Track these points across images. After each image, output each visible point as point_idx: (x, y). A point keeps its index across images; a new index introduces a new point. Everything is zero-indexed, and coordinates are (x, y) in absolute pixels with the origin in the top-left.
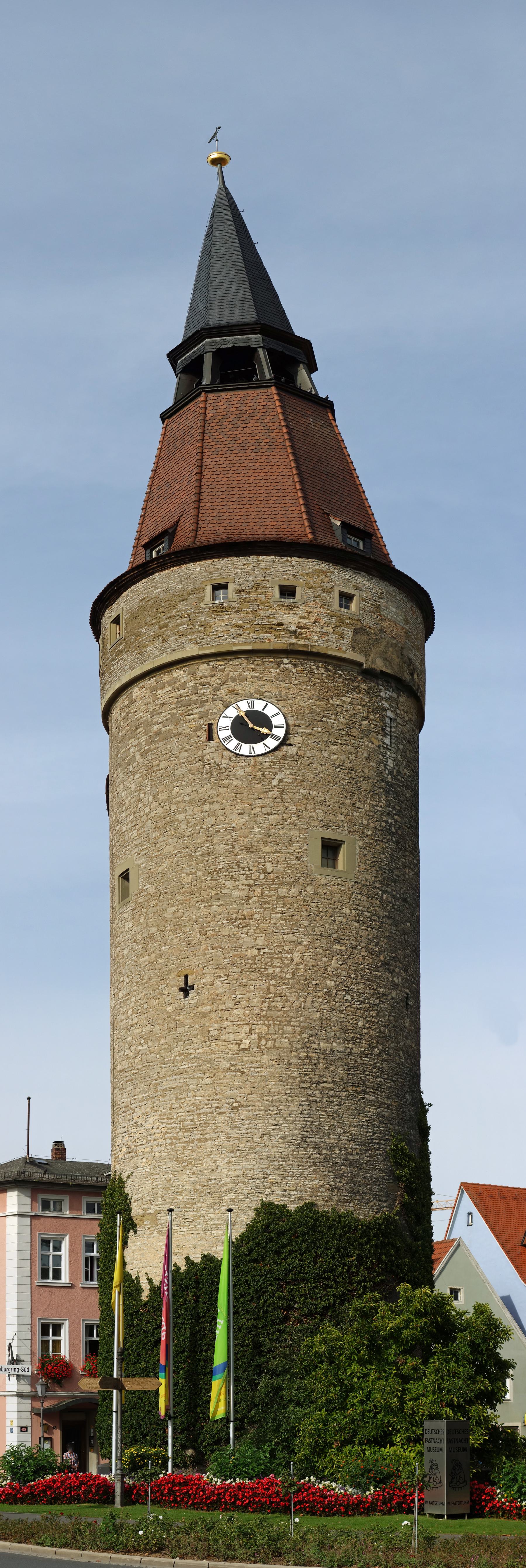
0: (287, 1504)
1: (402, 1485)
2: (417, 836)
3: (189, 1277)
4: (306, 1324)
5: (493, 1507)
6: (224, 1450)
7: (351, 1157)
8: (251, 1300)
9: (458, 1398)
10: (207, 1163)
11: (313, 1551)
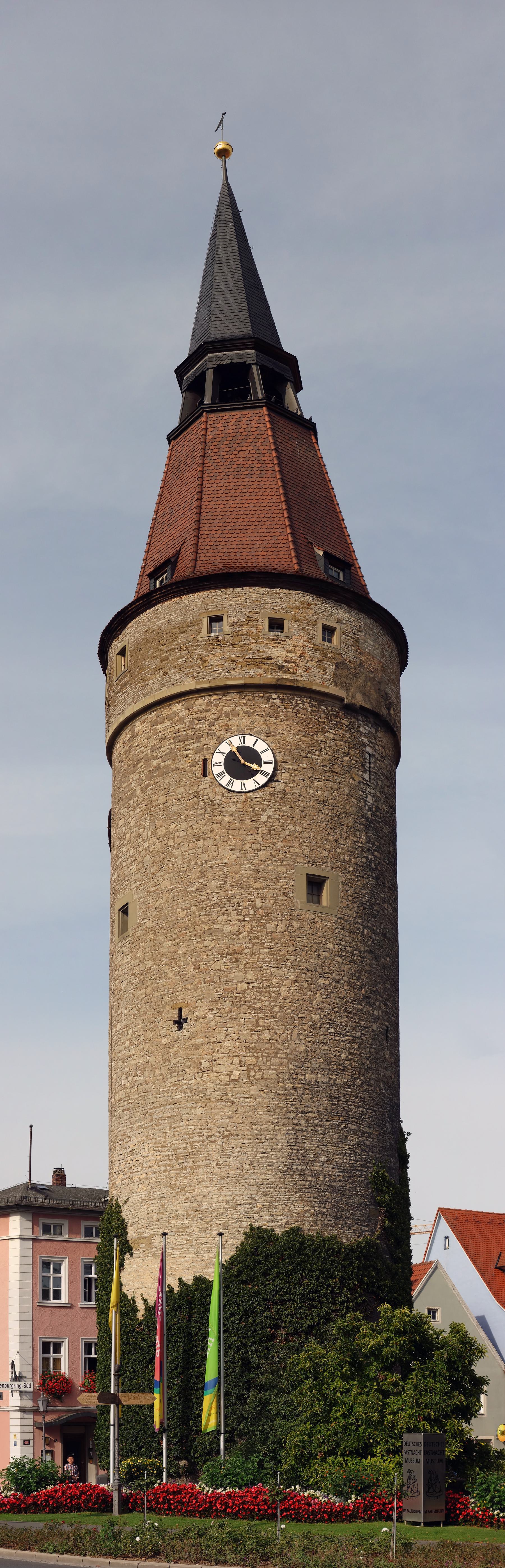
0: (274, 1511)
1: (381, 1494)
2: (395, 871)
3: (182, 1297)
4: (292, 1341)
5: (467, 1515)
6: (215, 1461)
7: (334, 1184)
8: (240, 1320)
9: (435, 1412)
10: (199, 1189)
11: (298, 1556)
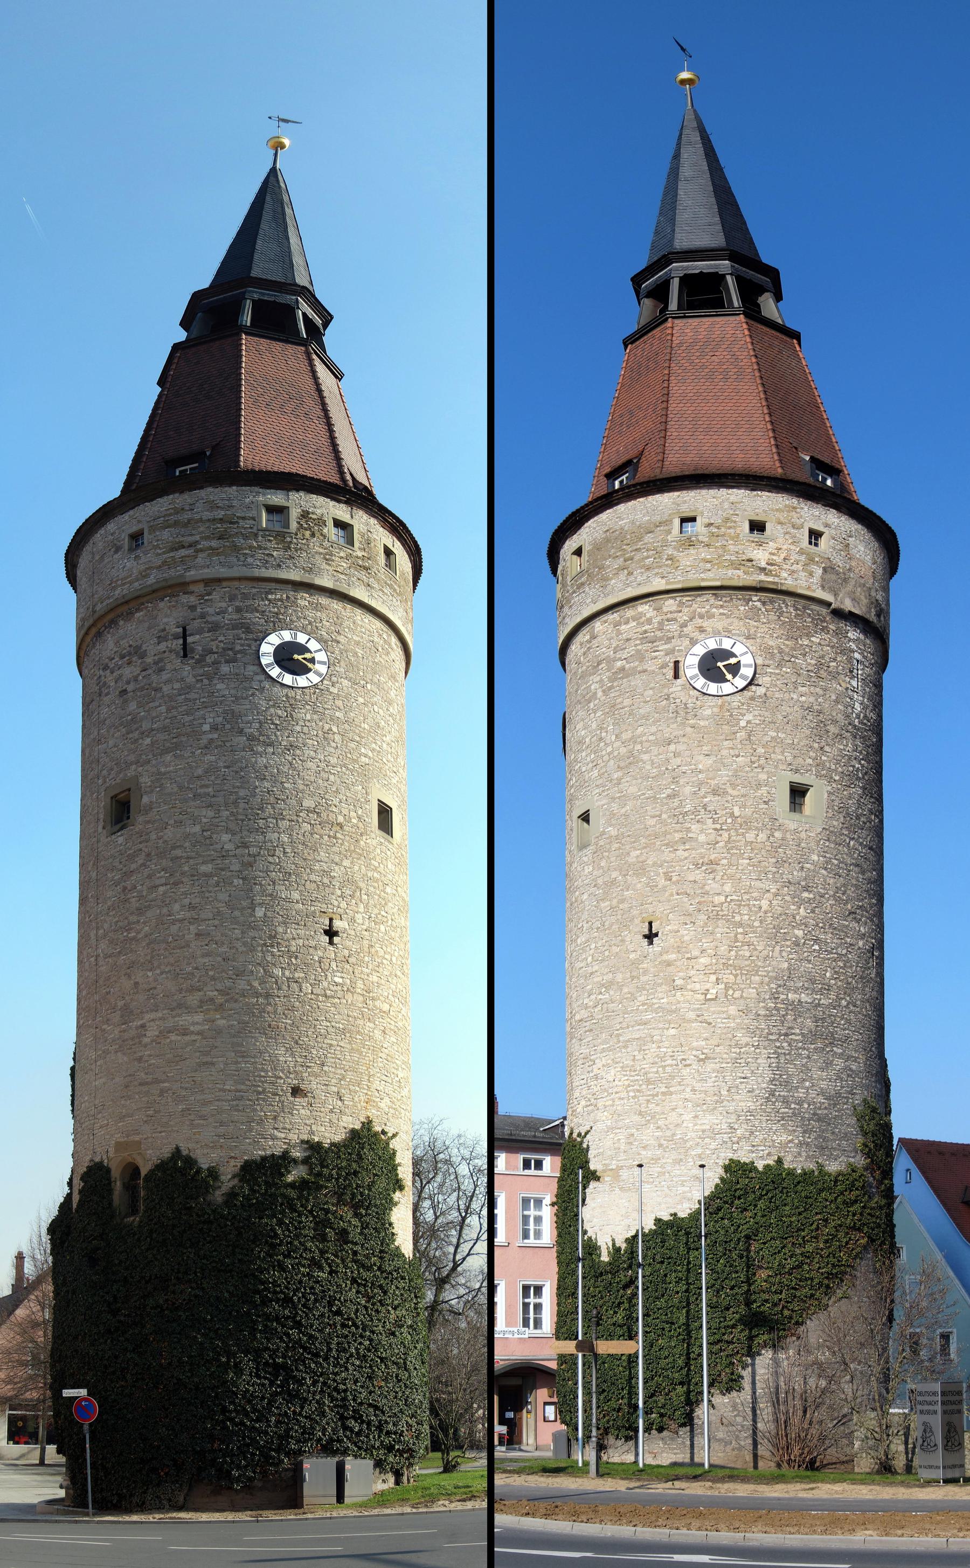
10: (673, 1117)
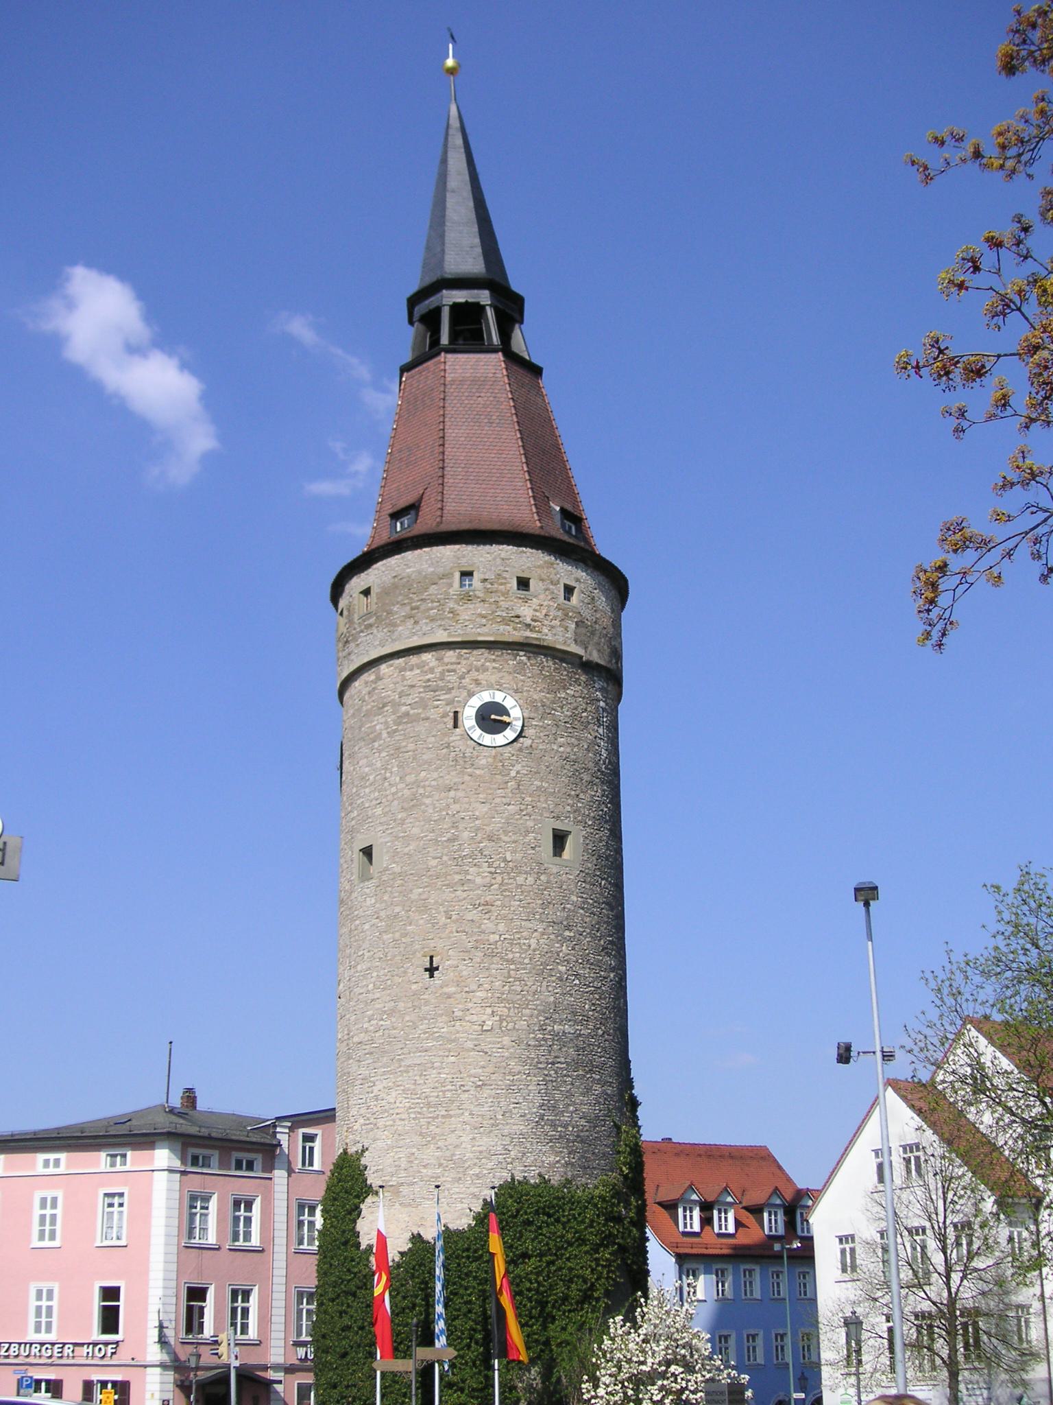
10: (452, 1139)
